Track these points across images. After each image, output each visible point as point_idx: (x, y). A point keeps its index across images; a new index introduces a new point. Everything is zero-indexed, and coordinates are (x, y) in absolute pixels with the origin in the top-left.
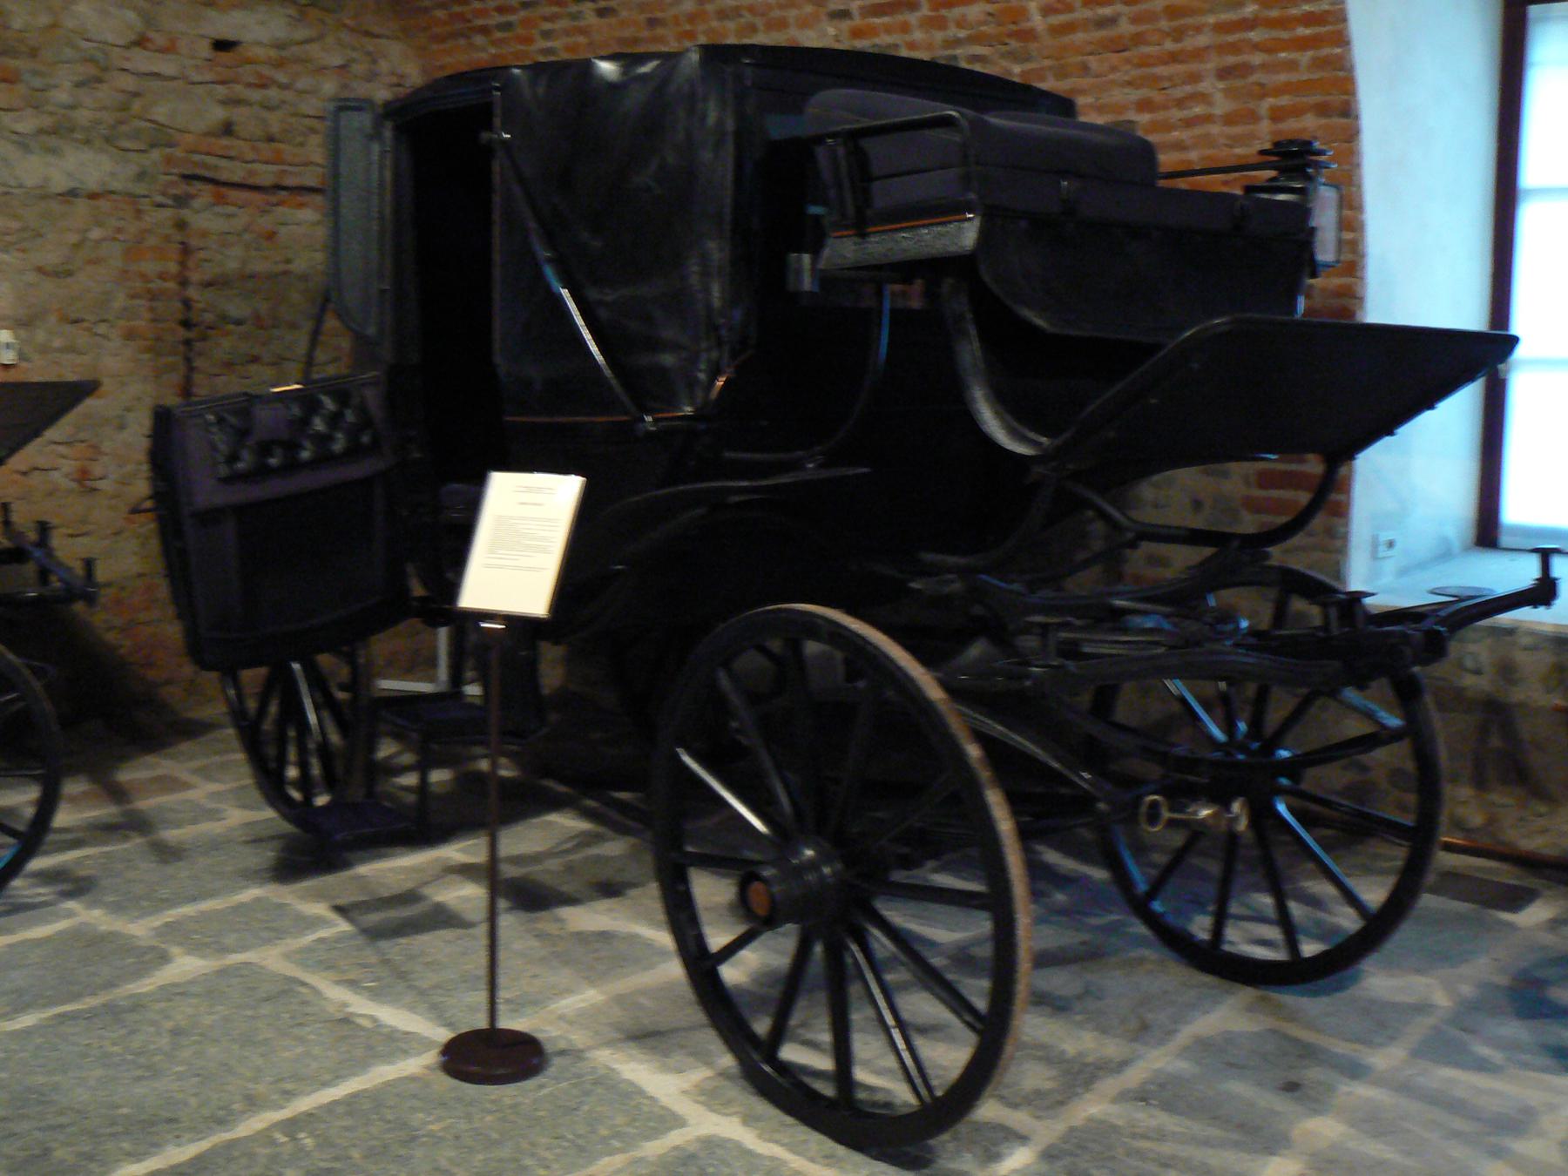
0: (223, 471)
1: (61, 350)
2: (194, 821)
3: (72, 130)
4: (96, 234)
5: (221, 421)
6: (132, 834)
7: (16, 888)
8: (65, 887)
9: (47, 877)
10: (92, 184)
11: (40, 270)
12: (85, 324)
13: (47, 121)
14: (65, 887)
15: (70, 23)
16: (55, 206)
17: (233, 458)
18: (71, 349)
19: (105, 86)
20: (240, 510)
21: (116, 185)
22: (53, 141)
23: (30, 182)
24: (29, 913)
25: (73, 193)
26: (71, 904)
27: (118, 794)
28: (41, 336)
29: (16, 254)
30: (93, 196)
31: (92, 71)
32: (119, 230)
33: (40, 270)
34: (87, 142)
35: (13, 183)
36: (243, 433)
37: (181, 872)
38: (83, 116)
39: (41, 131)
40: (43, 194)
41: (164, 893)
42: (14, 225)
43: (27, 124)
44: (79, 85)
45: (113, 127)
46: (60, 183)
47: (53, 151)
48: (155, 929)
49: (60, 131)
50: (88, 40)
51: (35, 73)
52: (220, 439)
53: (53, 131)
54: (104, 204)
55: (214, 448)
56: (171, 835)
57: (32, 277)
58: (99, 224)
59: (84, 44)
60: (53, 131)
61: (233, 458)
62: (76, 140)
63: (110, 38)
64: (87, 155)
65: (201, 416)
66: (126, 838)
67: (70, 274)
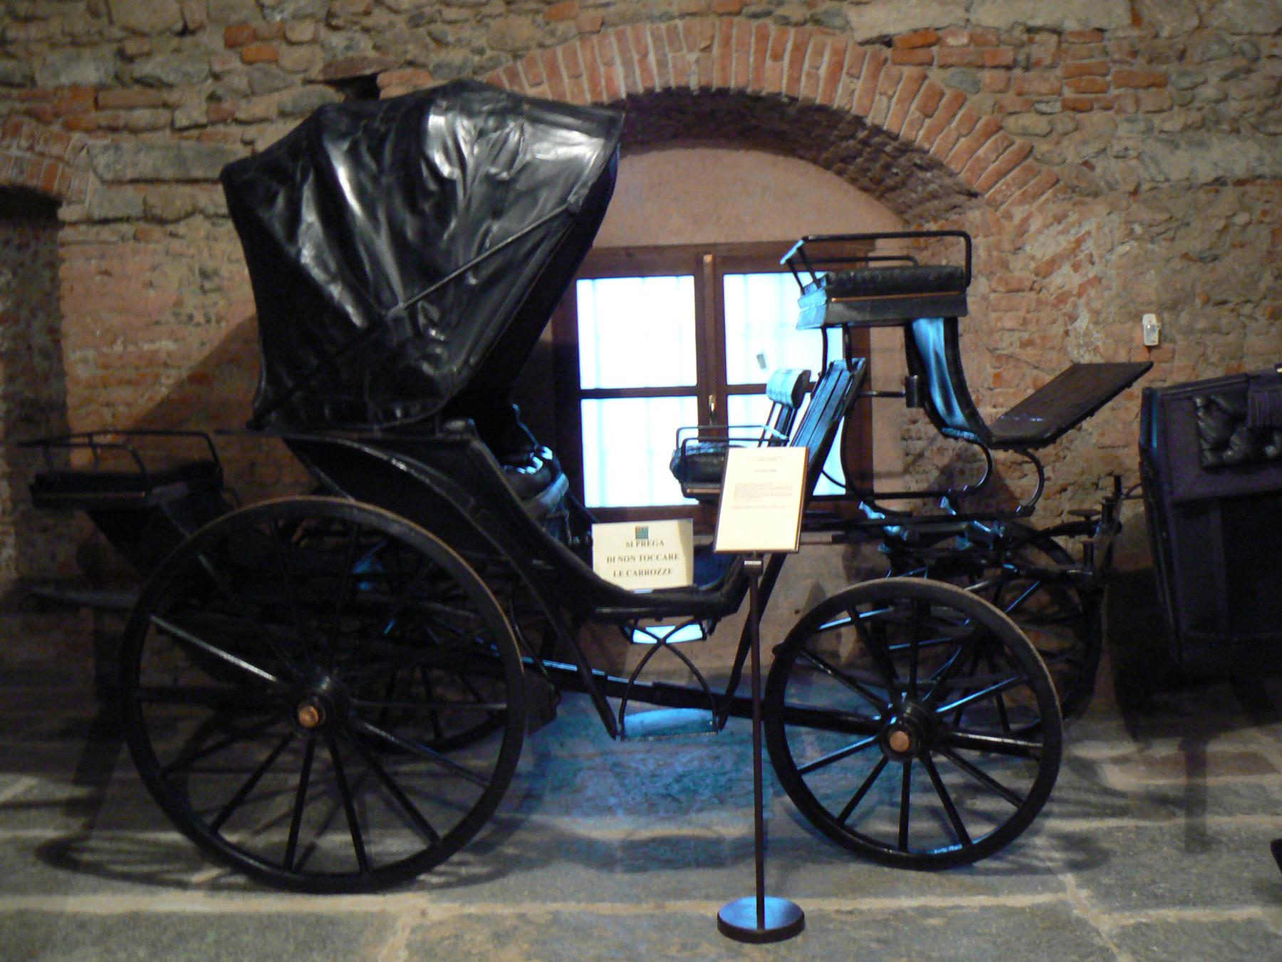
0: (1209, 457)
1: (1203, 331)
2: (1251, 810)
3: (1218, 122)
4: (1242, 218)
5: (1209, 405)
6: (1178, 812)
7: (1035, 847)
8: (1078, 856)
9: (1070, 842)
10: (1240, 171)
11: (1185, 256)
12: (1230, 306)
13: (1194, 117)
14: (1078, 856)
15: (1217, 21)
16: (1202, 196)
17: (1221, 445)
18: (1216, 330)
19: (1253, 76)
20: (1226, 502)
21: (1265, 170)
22: (1197, 135)
23: (1175, 175)
24: (1028, 878)
25: (1219, 182)
26: (1069, 879)
27: (1195, 764)
28: (1184, 318)
29: (1164, 244)
30: (1240, 183)
31: (1244, 63)
32: (1265, 213)
33: (1185, 256)
34: (1236, 131)
35: (1160, 178)
36: (1234, 420)
37: (1199, 865)
38: (1233, 107)
39: (1186, 128)
40: (1190, 186)
41: (1161, 888)
42: (1162, 217)
43: (1174, 122)
44: (1226, 79)
45: (1261, 114)
46: (1206, 173)
47: (1201, 144)
48: (1123, 927)
49: (1207, 124)
50: (1234, 34)
51: (1182, 74)
52: (1209, 425)
53: (1202, 125)
54: (1253, 190)
55: (1200, 433)
56: (1215, 822)
57: (1177, 264)
58: (1245, 208)
59: (1230, 39)
60: (1202, 125)
61: (1221, 445)
62: (1223, 131)
63: (1260, 28)
64: (1234, 144)
65: (1190, 398)
66: (1172, 815)
67: (1215, 258)
